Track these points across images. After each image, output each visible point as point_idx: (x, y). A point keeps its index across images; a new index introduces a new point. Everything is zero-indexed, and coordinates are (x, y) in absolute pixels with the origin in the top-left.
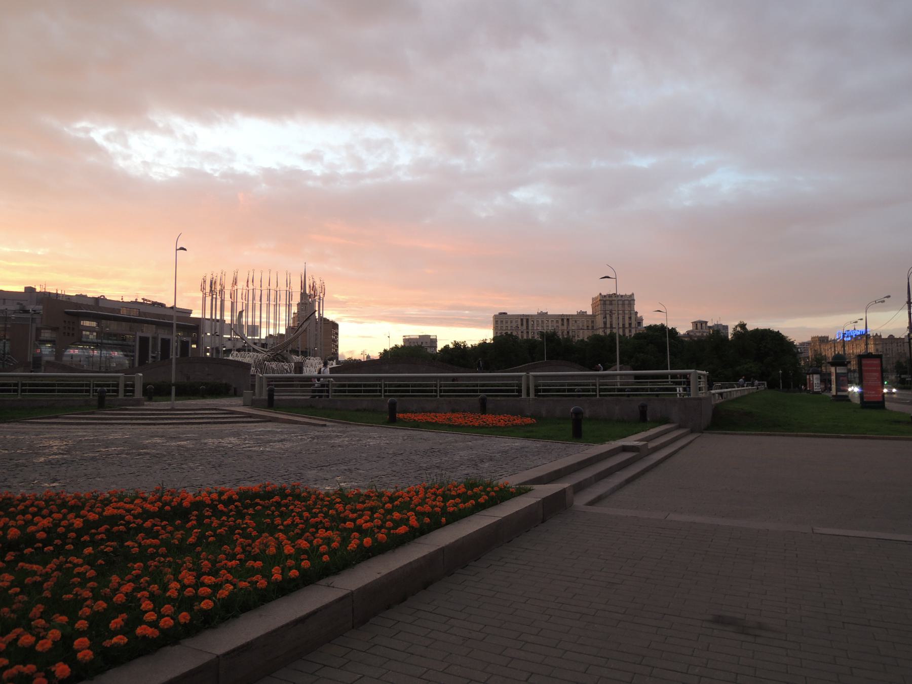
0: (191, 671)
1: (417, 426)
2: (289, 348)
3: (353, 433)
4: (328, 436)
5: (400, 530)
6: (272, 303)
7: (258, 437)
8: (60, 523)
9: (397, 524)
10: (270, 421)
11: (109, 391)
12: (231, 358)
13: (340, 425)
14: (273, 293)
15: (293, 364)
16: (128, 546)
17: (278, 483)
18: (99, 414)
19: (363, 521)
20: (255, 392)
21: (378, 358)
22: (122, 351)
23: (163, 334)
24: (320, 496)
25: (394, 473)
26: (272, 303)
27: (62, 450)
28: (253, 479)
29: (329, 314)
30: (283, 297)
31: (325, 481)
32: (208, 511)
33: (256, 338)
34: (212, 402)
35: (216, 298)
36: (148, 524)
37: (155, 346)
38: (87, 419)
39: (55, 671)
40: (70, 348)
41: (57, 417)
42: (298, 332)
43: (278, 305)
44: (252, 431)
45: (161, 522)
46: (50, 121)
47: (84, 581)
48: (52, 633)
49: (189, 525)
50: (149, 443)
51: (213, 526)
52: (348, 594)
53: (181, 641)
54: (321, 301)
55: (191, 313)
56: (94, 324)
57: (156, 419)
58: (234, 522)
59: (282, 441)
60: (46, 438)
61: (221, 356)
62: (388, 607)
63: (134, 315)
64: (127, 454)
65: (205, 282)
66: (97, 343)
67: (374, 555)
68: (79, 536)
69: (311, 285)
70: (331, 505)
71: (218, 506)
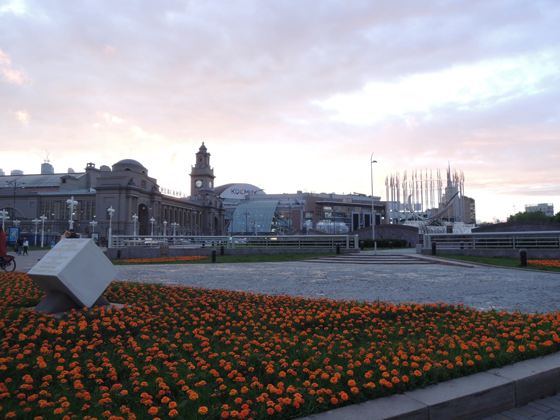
0: (413, 412)
1: (544, 269)
2: (442, 217)
3: (494, 272)
4: (476, 274)
5: (546, 343)
6: (429, 188)
7: (429, 273)
8: (329, 315)
9: (543, 338)
10: (434, 263)
11: (341, 245)
12: (405, 224)
13: (483, 267)
14: (429, 183)
15: (446, 227)
16: (366, 332)
17: (448, 303)
18: (337, 257)
19: (515, 334)
20: (423, 245)
21: (506, 221)
22: (345, 222)
23: (366, 212)
24: (479, 314)
25: (531, 302)
26: (429, 188)
27: (323, 276)
28: (430, 299)
29: (468, 193)
30: (436, 185)
31: (479, 304)
32: (406, 316)
33: (420, 211)
34: (397, 251)
35: (394, 189)
36: (374, 320)
37: (361, 219)
38: (332, 260)
39: (341, 395)
40: (320, 222)
41: (317, 259)
42: (447, 206)
43: (433, 190)
44: (424, 269)
45: (381, 320)
46: (316, 102)
47: (347, 349)
48: (337, 375)
49: (397, 324)
50: (366, 274)
51: (412, 325)
52: (512, 382)
53: (405, 393)
54: (462, 185)
55: (380, 199)
56: (330, 208)
57: (367, 260)
58: (424, 324)
59: (445, 276)
60: (314, 270)
61: (399, 223)
62: (542, 398)
63: (350, 202)
64: (356, 280)
65: (387, 180)
66: (332, 219)
67: (527, 358)
68: (339, 324)
69: (454, 176)
70: (488, 320)
71: (413, 314)
